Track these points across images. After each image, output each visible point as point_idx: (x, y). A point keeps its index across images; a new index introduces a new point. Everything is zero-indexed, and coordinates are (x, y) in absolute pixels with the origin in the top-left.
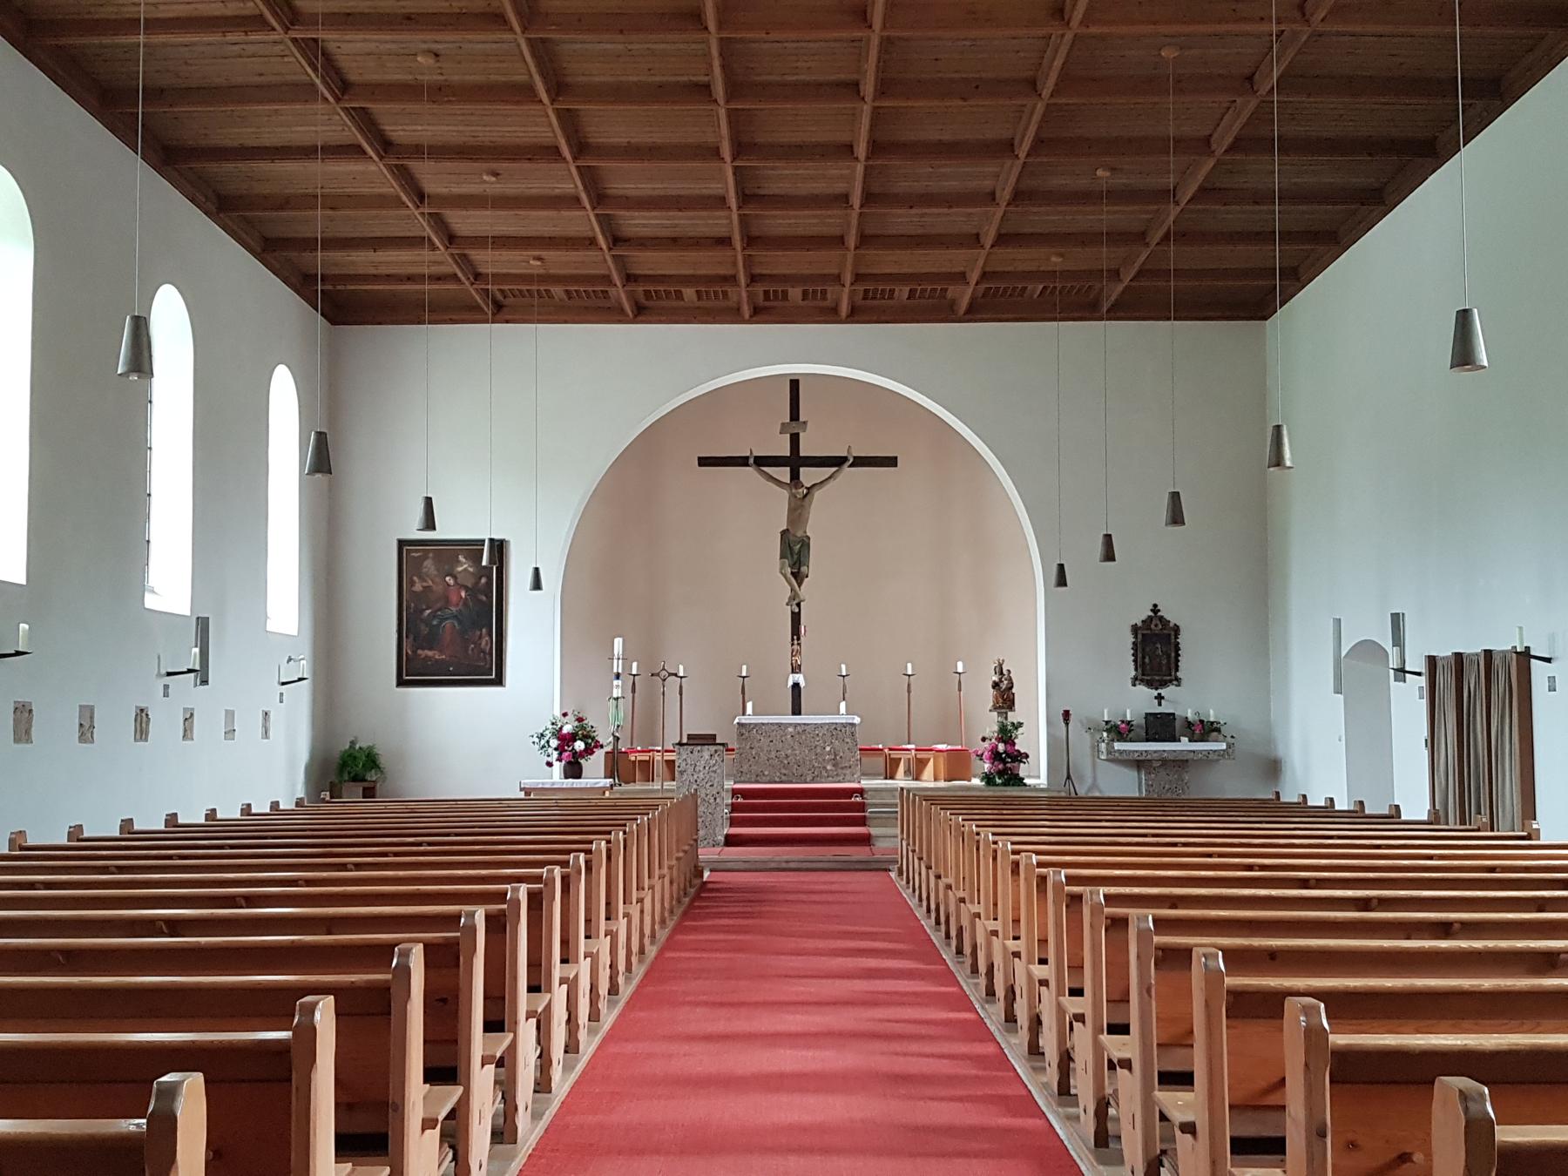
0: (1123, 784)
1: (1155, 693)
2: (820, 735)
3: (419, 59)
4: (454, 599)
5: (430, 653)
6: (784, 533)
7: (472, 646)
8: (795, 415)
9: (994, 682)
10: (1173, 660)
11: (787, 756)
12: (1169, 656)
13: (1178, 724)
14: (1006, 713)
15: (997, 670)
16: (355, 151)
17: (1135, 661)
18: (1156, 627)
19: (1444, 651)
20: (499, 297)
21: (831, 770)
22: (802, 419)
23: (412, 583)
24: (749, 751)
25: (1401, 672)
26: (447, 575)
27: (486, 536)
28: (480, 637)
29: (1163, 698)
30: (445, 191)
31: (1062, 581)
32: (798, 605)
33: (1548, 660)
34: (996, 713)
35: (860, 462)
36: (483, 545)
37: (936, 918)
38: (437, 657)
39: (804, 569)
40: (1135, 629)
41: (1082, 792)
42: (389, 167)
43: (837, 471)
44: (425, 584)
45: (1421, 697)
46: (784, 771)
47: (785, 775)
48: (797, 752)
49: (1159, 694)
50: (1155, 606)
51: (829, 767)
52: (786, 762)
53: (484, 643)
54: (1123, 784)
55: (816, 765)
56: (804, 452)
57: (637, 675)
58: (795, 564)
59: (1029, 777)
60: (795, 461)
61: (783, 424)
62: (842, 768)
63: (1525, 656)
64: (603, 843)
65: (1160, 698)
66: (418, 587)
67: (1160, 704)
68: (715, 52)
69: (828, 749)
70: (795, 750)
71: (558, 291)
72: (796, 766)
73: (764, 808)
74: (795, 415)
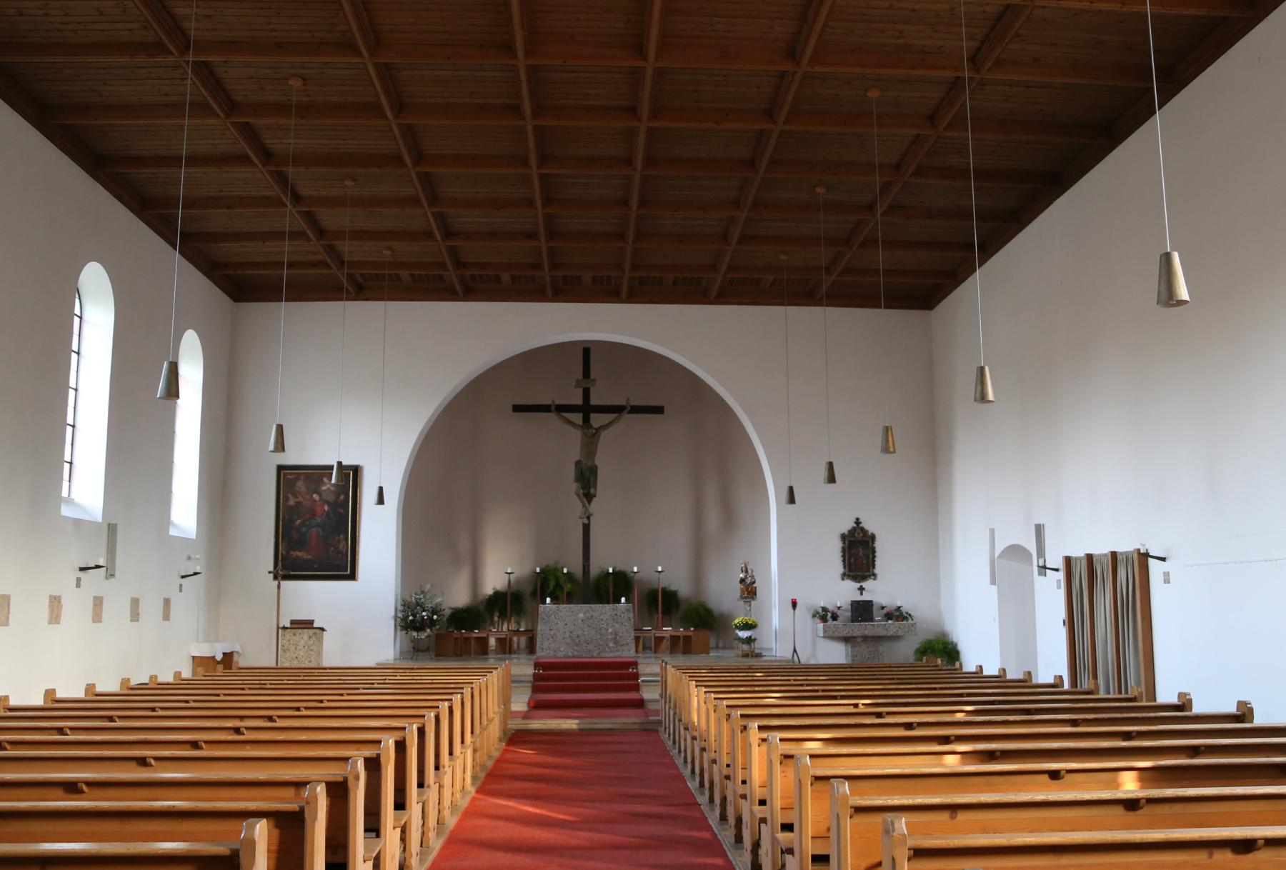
0: (835, 654)
1: (858, 585)
2: (605, 619)
3: (290, 82)
4: (319, 511)
5: (299, 554)
6: (578, 463)
7: (332, 549)
8: (586, 373)
9: (742, 578)
10: (871, 560)
11: (578, 636)
12: (868, 557)
13: (875, 608)
14: (750, 602)
15: (744, 569)
16: (243, 159)
17: (844, 561)
18: (859, 535)
19: (1078, 552)
20: (360, 280)
22: (592, 377)
23: (286, 499)
25: (1043, 569)
26: (314, 493)
27: (333, 462)
28: (339, 541)
29: (864, 589)
30: (315, 193)
31: (792, 500)
32: (588, 518)
33: (1163, 559)
34: (743, 603)
35: (637, 410)
36: (333, 469)
37: (700, 782)
38: (305, 557)
39: (592, 491)
40: (843, 537)
41: (803, 661)
42: (271, 173)
43: (616, 418)
44: (297, 500)
45: (1059, 587)
46: (575, 648)
47: (576, 650)
48: (586, 633)
49: (861, 586)
50: (858, 519)
51: (611, 645)
52: (577, 640)
53: (341, 547)
54: (835, 654)
56: (595, 400)
57: (511, 573)
60: (587, 409)
61: (577, 381)
62: (621, 645)
63: (1144, 557)
64: (469, 689)
65: (861, 589)
66: (292, 502)
67: (861, 594)
68: (523, 77)
69: (610, 630)
70: (584, 631)
71: (404, 274)
72: (585, 644)
73: (561, 678)
74: (586, 373)
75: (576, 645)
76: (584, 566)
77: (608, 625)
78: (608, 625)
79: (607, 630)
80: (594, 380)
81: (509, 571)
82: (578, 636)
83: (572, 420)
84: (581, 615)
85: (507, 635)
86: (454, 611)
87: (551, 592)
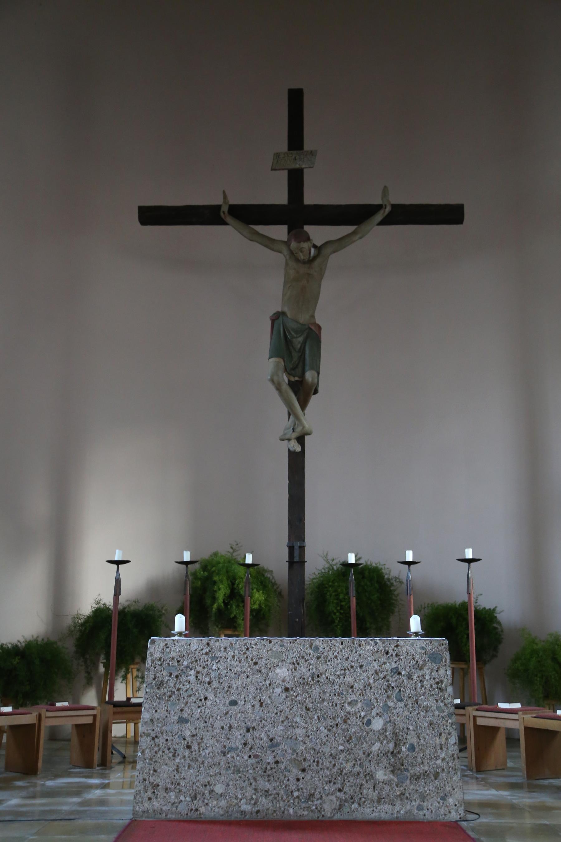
6: (277, 318)
11: (273, 743)
21: (388, 783)
22: (307, 146)
24: (175, 728)
32: (301, 440)
39: (309, 376)
43: (354, 233)
46: (263, 784)
47: (267, 793)
51: (380, 775)
55: (348, 767)
58: (294, 369)
59: (133, 697)
61: (277, 156)
62: (417, 778)
69: (378, 724)
72: (295, 771)
75: (267, 774)
76: (291, 549)
77: (370, 705)
78: (370, 705)
79: (369, 723)
80: (312, 153)
81: (117, 558)
82: (273, 743)
83: (261, 232)
84: (282, 672)
85: (95, 716)
86: (27, 643)
87: (219, 610)
